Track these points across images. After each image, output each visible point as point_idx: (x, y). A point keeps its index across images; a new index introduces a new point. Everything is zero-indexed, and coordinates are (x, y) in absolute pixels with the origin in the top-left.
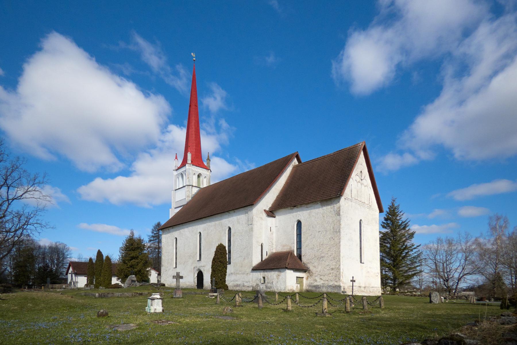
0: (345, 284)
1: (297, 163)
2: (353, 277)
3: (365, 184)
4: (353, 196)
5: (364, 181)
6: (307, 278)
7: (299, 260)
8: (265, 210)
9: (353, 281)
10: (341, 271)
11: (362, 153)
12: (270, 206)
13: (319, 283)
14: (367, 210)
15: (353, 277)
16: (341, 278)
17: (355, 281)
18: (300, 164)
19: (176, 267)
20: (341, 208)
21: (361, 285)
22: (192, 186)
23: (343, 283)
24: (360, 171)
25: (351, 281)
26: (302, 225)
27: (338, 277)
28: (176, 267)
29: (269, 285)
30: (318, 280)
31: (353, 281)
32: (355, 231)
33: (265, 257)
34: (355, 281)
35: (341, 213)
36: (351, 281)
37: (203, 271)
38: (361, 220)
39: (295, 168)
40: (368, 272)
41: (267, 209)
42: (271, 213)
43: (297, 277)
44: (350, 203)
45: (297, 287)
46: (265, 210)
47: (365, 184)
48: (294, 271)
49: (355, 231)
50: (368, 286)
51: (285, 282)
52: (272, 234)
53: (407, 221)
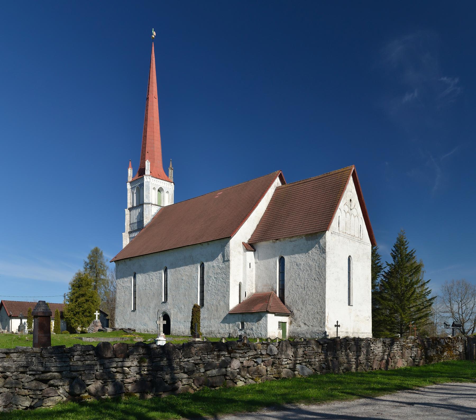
0: (330, 329)
1: (280, 184)
2: (337, 322)
3: (355, 214)
4: (341, 229)
5: (354, 210)
6: (291, 323)
7: (281, 303)
8: (243, 243)
9: (337, 326)
10: (327, 315)
11: (351, 178)
12: (249, 237)
13: (304, 328)
14: (357, 244)
15: (337, 322)
16: (326, 323)
17: (339, 326)
18: (284, 186)
19: (135, 310)
20: (327, 244)
21: (349, 330)
22: (152, 204)
23: (328, 328)
24: (349, 199)
25: (335, 326)
26: (286, 261)
27: (322, 322)
28: (135, 310)
29: (248, 331)
30: (302, 325)
31: (337, 326)
32: (342, 269)
33: (243, 298)
34: (339, 326)
35: (327, 250)
36: (335, 326)
37: (169, 313)
38: (350, 257)
39: (277, 189)
40: (357, 316)
41: (246, 241)
42: (251, 246)
43: (279, 322)
44: (337, 237)
45: (279, 333)
46: (243, 243)
47: (355, 214)
48: (275, 315)
49: (342, 269)
50: (356, 331)
51: (266, 330)
52: (252, 271)
53: (414, 251)
